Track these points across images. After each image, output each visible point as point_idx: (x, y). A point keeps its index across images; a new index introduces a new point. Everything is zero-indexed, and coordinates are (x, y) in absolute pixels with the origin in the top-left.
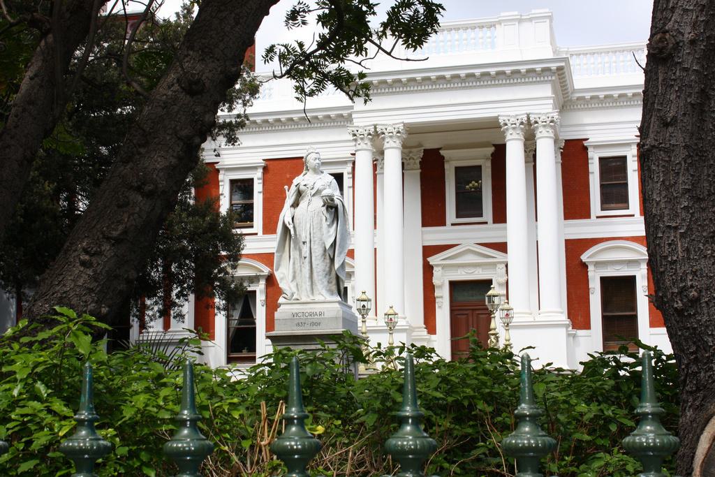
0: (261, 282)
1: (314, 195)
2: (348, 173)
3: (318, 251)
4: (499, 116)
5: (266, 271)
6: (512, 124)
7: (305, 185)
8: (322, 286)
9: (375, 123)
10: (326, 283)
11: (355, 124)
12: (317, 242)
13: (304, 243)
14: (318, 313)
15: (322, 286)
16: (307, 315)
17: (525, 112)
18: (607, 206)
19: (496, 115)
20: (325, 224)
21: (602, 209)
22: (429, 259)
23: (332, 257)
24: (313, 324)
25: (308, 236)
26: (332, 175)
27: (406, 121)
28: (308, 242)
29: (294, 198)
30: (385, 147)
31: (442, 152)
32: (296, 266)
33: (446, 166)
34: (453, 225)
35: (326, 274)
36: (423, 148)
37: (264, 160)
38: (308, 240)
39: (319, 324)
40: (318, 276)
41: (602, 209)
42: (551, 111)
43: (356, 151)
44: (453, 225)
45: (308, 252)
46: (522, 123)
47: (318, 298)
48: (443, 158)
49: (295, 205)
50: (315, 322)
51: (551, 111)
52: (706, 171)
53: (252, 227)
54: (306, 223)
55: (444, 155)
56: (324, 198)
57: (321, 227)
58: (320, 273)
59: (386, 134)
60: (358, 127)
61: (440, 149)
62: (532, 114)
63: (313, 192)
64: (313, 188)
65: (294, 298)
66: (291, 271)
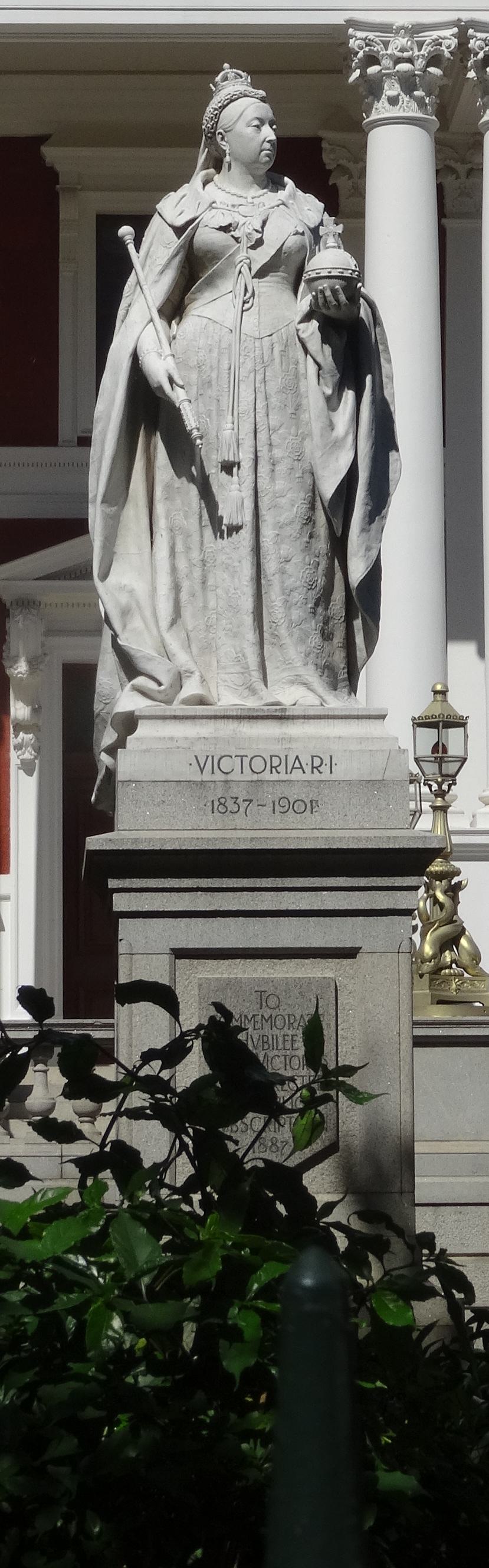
1: (261, 274)
6: (398, 61)
7: (225, 229)
8: (302, 648)
10: (315, 639)
12: (282, 468)
13: (228, 468)
14: (305, 760)
15: (302, 648)
16: (258, 765)
18: (66, 429)
23: (339, 533)
24: (287, 805)
25: (248, 443)
26: (204, 189)
28: (247, 464)
29: (168, 279)
31: (50, 153)
33: (67, 211)
35: (317, 604)
38: (245, 458)
39: (313, 805)
40: (287, 605)
45: (249, 505)
46: (434, 60)
48: (52, 175)
50: (293, 794)
56: (325, 284)
57: (298, 407)
58: (297, 597)
61: (43, 139)
63: (262, 256)
64: (259, 243)
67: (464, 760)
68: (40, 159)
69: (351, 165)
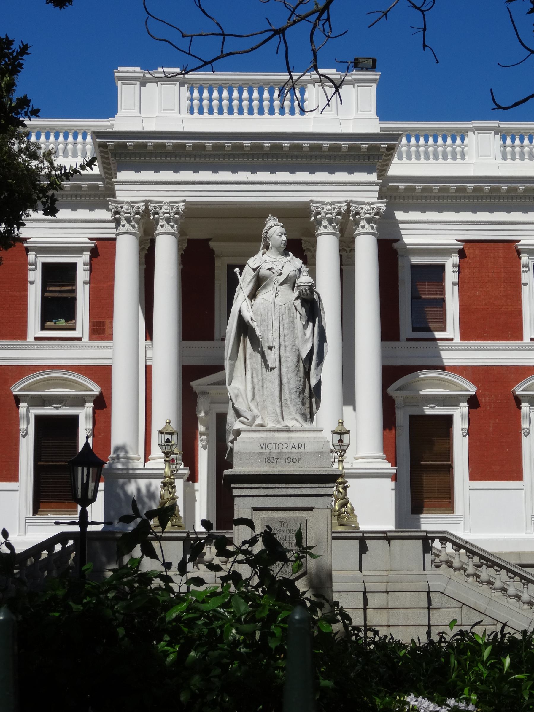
0: (87, 404)
1: (282, 284)
2: (85, 264)
3: (289, 361)
4: (311, 201)
5: (96, 390)
6: (327, 214)
8: (295, 408)
9: (147, 198)
10: (299, 405)
11: (118, 199)
13: (271, 348)
14: (296, 445)
15: (295, 408)
17: (345, 199)
19: (307, 200)
20: (299, 323)
21: (43, 328)
22: (193, 384)
24: (290, 460)
27: (188, 200)
28: (277, 347)
30: (157, 232)
31: (212, 244)
32: (255, 380)
33: (217, 263)
34: (408, 340)
35: (300, 393)
36: (188, 237)
37: (89, 239)
38: (276, 345)
39: (299, 460)
40: (290, 394)
41: (43, 328)
42: (376, 200)
43: (117, 235)
44: (408, 340)
45: (278, 360)
47: (291, 424)
48: (212, 252)
49: (253, 296)
51: (376, 200)
52: (510, 292)
53: (74, 329)
54: (273, 320)
55: (214, 249)
56: (303, 288)
57: (294, 328)
58: (293, 391)
59: (161, 214)
60: (122, 202)
61: (209, 240)
62: (354, 202)
65: (256, 423)
66: (249, 386)
67: (349, 445)
68: (208, 246)
69: (311, 248)
